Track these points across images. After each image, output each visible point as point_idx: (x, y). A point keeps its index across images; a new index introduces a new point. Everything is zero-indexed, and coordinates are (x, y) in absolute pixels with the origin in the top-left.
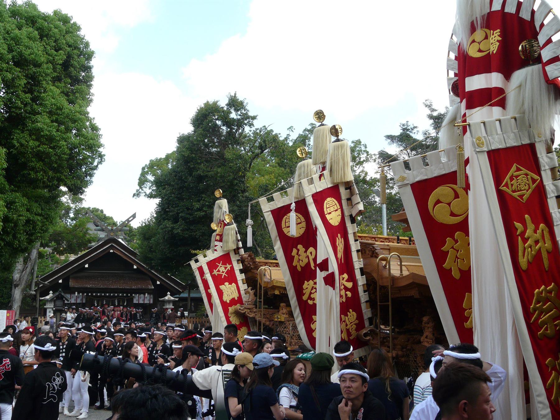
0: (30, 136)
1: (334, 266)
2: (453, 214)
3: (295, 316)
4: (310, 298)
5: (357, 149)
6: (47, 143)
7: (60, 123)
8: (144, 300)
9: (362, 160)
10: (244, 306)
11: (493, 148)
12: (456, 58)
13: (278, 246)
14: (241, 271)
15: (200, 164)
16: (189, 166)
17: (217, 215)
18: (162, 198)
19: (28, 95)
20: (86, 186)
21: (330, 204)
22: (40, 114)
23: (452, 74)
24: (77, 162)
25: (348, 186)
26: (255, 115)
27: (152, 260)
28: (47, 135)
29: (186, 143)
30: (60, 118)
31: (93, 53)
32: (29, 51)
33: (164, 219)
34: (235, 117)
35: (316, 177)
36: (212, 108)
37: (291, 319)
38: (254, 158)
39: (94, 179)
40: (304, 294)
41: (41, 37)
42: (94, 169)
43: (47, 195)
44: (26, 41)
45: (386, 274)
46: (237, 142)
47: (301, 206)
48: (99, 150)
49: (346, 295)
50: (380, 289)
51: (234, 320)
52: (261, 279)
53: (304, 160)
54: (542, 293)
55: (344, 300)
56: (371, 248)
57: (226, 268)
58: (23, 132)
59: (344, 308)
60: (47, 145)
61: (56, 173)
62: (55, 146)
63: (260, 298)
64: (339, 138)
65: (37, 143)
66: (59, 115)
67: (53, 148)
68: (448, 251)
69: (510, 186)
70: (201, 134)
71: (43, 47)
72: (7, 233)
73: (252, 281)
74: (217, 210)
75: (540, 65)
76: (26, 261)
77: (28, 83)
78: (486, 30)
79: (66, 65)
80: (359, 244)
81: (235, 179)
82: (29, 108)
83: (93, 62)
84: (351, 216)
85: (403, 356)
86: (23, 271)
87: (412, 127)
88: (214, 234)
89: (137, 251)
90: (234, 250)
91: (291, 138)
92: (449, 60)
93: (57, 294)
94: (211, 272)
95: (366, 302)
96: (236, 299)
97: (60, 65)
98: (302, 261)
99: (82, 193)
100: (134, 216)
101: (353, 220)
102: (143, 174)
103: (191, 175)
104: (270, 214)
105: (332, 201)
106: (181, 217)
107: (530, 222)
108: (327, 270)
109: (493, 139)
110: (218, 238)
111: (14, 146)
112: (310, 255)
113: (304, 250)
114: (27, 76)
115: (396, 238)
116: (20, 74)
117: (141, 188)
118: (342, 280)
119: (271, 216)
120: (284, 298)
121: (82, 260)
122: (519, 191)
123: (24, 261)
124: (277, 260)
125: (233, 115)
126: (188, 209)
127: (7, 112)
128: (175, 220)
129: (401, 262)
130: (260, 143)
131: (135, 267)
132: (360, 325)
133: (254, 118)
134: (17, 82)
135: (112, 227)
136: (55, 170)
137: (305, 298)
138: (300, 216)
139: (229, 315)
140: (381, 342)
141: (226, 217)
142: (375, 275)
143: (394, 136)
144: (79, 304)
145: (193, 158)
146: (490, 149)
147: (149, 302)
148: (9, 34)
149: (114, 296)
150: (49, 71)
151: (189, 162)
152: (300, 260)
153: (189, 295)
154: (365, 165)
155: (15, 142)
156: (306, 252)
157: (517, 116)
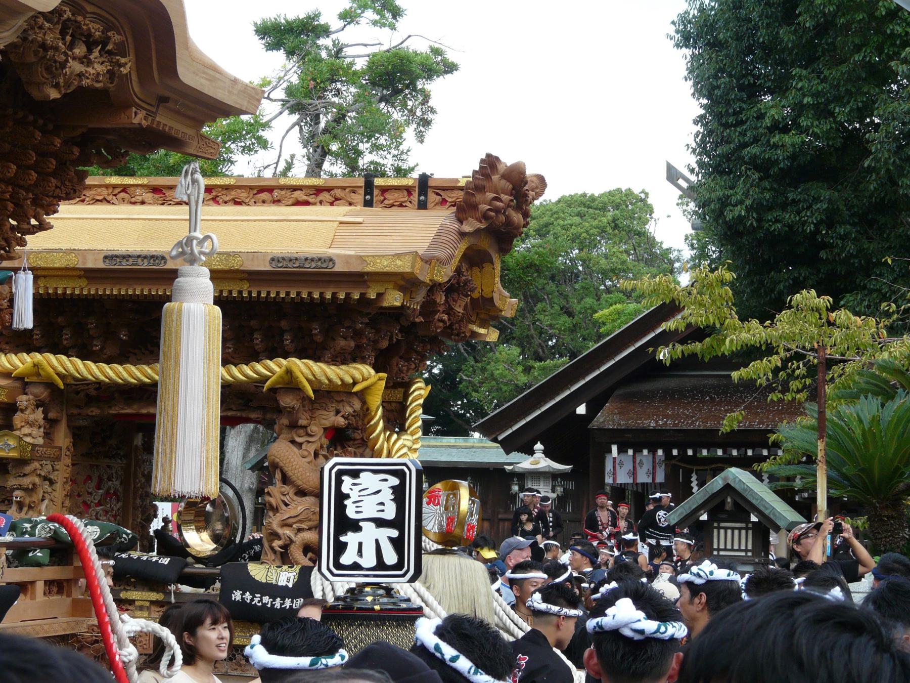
8: (634, 473)
115: (361, 182)
121: (645, 335)
147: (631, 481)
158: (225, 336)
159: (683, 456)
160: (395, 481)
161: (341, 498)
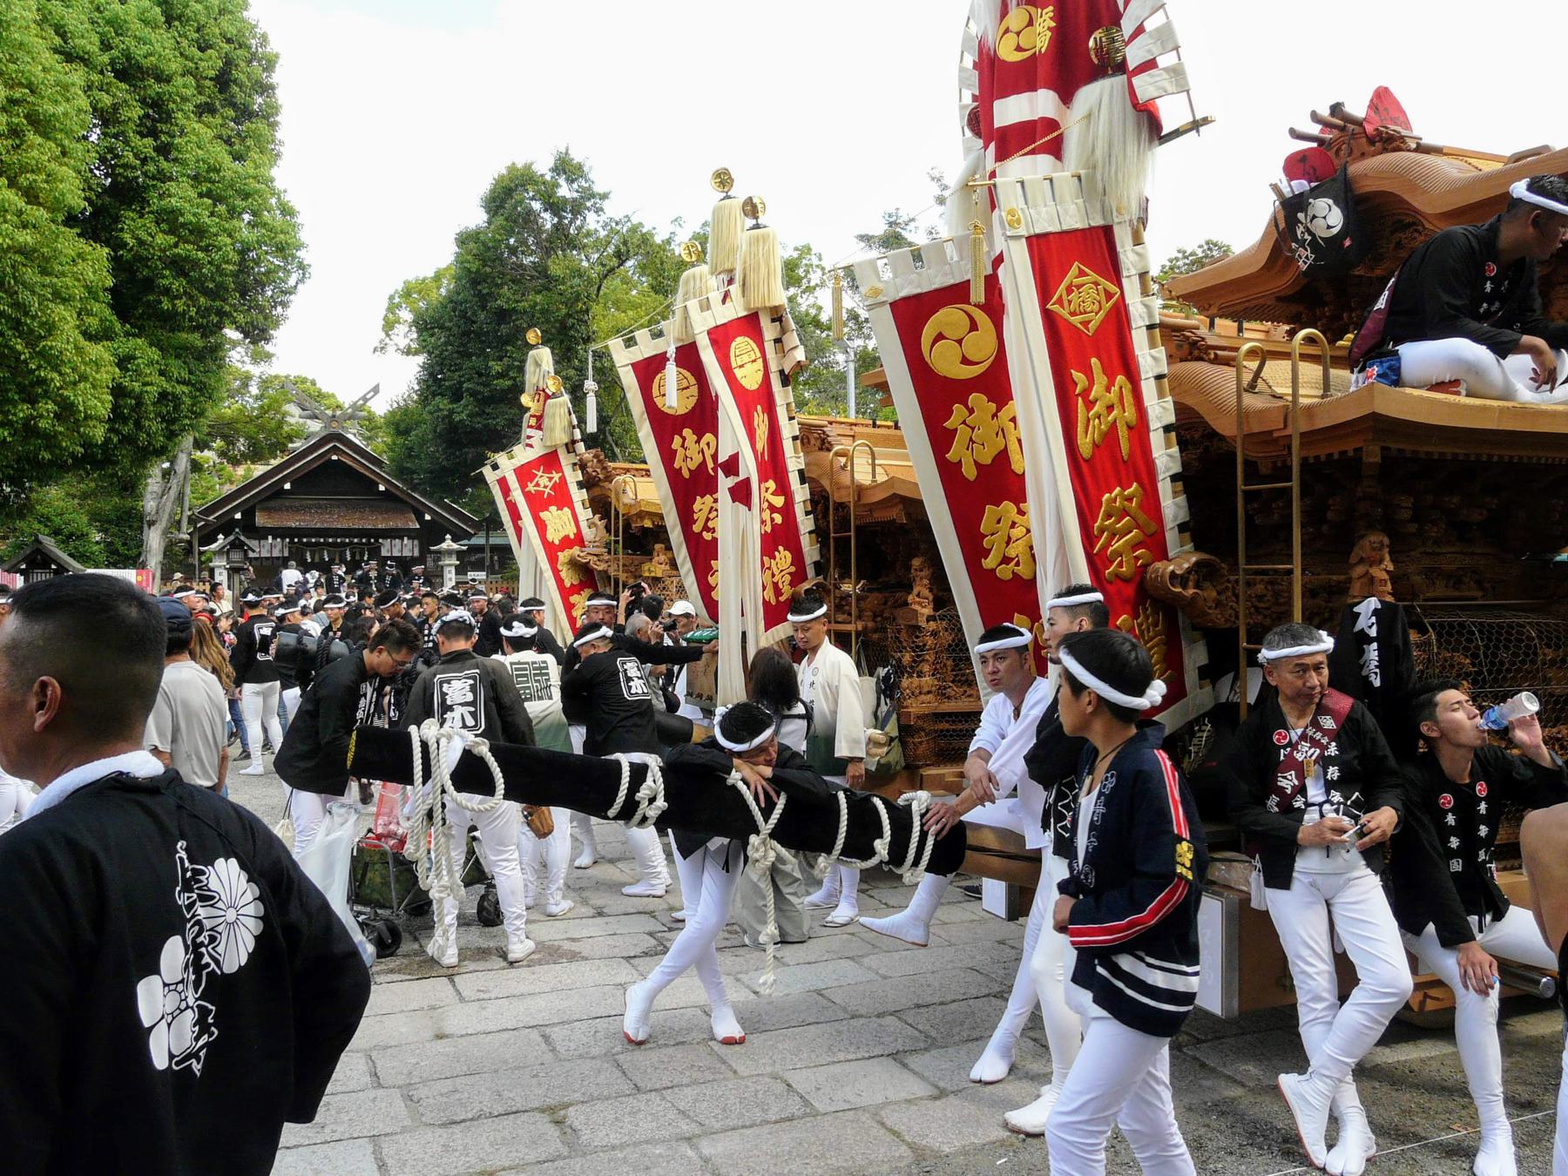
0: (157, 223)
1: (749, 467)
2: (965, 361)
3: (679, 562)
4: (706, 528)
5: (804, 262)
6: (192, 238)
7: (218, 199)
9: (812, 284)
10: (587, 550)
11: (1038, 231)
12: (976, 66)
13: (645, 433)
14: (581, 485)
15: (500, 286)
16: (480, 291)
17: (531, 377)
18: (430, 353)
19: (149, 141)
20: (276, 325)
22: (176, 180)
23: (967, 99)
24: (255, 279)
25: (777, 316)
26: (607, 191)
27: (414, 472)
28: (191, 223)
29: (472, 245)
30: (217, 188)
31: (277, 56)
32: (144, 49)
33: (434, 395)
34: (568, 195)
35: (715, 297)
36: (522, 175)
37: (675, 572)
38: (606, 276)
39: (289, 312)
40: (695, 523)
41: (169, 20)
42: (291, 293)
43: (199, 343)
44: (136, 26)
45: (845, 479)
46: (572, 244)
47: (688, 356)
48: (298, 254)
49: (772, 520)
50: (836, 509)
51: (569, 578)
52: (618, 500)
53: (693, 266)
54: (1115, 500)
55: (768, 528)
57: (550, 479)
58: (142, 216)
59: (770, 544)
60: (193, 243)
61: (214, 300)
62: (209, 245)
63: (617, 535)
64: (760, 221)
65: (172, 239)
66: (213, 182)
67: (206, 249)
68: (956, 430)
69: (1066, 304)
70: (503, 228)
71: (173, 41)
72: (125, 420)
73: (601, 506)
74: (532, 369)
75: (1125, 76)
76: (166, 474)
77: (147, 116)
78: (1029, 8)
79: (223, 80)
80: (797, 427)
81: (570, 316)
82: (151, 168)
83: (276, 78)
84: (782, 372)
85: (875, 630)
86: (163, 495)
87: (906, 219)
88: (527, 415)
89: (385, 458)
90: (566, 445)
91: (678, 239)
92: (962, 70)
93: (232, 538)
94: (523, 486)
95: (810, 532)
96: (572, 537)
97: (211, 79)
99: (267, 340)
100: (376, 390)
101: (786, 380)
102: (392, 308)
103: (484, 308)
106: (468, 390)
107: (1100, 371)
108: (737, 474)
109: (1039, 213)
110: (533, 422)
111: (126, 244)
112: (706, 448)
114: (143, 101)
116: (128, 97)
117: (388, 335)
118: (764, 493)
119: (632, 374)
120: (659, 533)
122: (1081, 313)
123: (164, 476)
124: (645, 463)
125: (565, 191)
126: (480, 375)
127: (107, 175)
128: (456, 396)
129: (874, 458)
130: (617, 246)
131: (382, 488)
132: (798, 576)
133: (604, 197)
134: (125, 114)
135: (334, 410)
136: (211, 294)
137: (697, 528)
138: (687, 374)
139: (560, 568)
140: (836, 606)
141: (550, 382)
142: (826, 483)
143: (873, 237)
144: (278, 558)
145: (487, 275)
146: (1032, 233)
148: (101, 12)
149: (344, 545)
150: (188, 92)
151: (479, 283)
153: (487, 540)
154: (818, 292)
155: (127, 237)
156: (698, 442)
157: (1082, 172)
158: (1051, 237)
159: (300, 542)
160: (472, 682)
161: (444, 695)
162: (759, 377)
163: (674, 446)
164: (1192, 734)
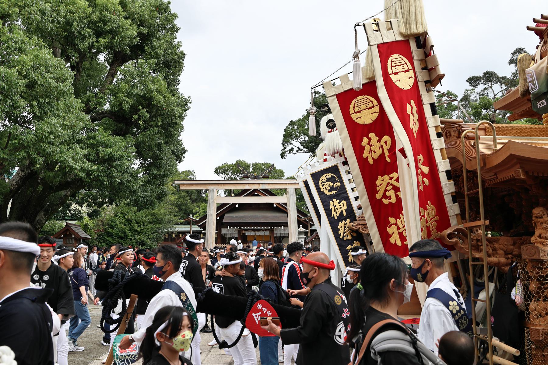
4: (385, 196)
21: (396, 62)
40: (377, 192)
45: (474, 153)
55: (421, 188)
56: (457, 127)
98: (375, 152)
104: (334, 99)
105: (401, 59)
112: (384, 145)
113: (377, 138)
119: (336, 101)
137: (378, 196)
152: (371, 151)
156: (379, 141)
162: (411, 82)
163: (363, 144)
164: (323, 193)
